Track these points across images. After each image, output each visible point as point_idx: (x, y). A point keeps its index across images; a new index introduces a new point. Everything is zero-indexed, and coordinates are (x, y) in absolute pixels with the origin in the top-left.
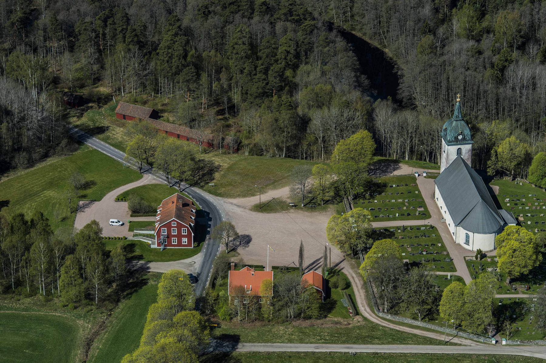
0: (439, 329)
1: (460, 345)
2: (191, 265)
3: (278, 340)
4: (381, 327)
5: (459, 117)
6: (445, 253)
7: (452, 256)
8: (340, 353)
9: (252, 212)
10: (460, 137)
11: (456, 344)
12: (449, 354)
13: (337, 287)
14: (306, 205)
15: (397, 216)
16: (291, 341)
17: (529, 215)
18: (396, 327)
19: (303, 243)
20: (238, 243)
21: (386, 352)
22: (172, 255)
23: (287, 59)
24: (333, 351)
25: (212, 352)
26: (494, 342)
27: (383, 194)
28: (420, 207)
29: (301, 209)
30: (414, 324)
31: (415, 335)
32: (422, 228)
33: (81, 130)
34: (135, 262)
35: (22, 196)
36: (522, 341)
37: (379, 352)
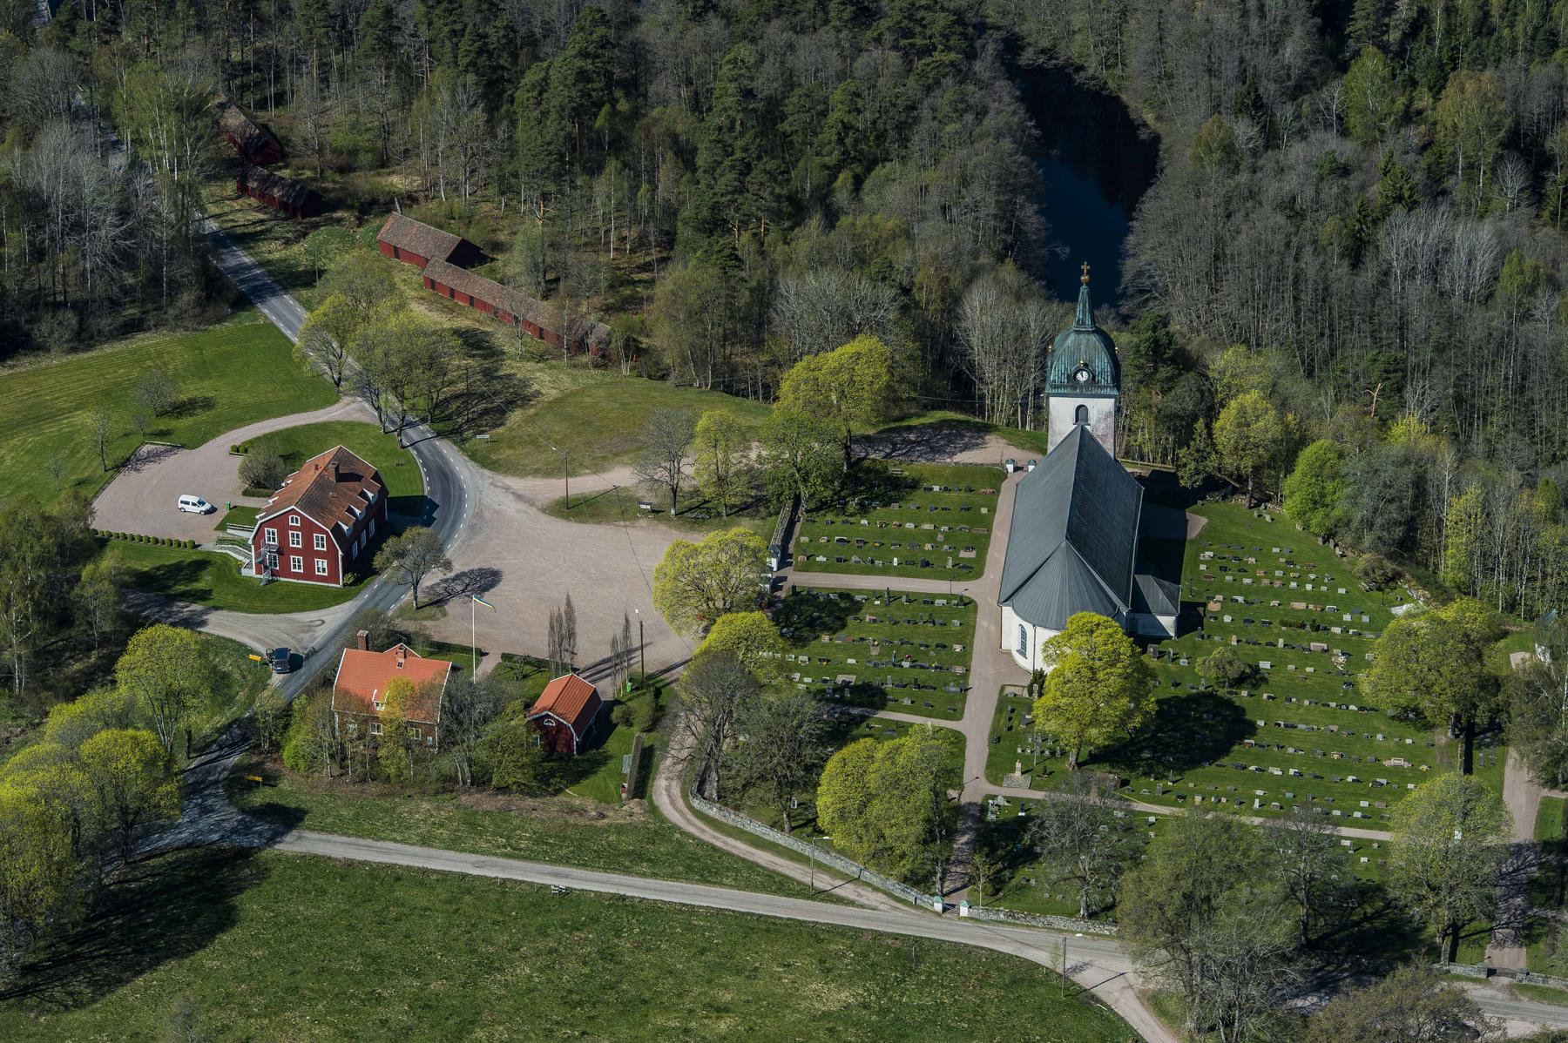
0: (819, 856)
1: (851, 903)
2: (309, 627)
3: (394, 835)
4: (678, 835)
5: (1084, 323)
6: (959, 670)
7: (973, 681)
8: (531, 884)
9: (545, 518)
10: (1083, 377)
11: (840, 900)
12: (805, 922)
13: (631, 725)
14: (682, 513)
15: (895, 563)
16: (425, 841)
17: (1241, 599)
18: (717, 839)
19: (574, 603)
20: (459, 588)
21: (647, 896)
22: (282, 599)
23: (844, 145)
24: (515, 877)
25: (214, 843)
26: (938, 907)
27: (895, 506)
28: (967, 549)
29: (669, 519)
30: (766, 837)
31: (752, 866)
32: (939, 602)
33: (270, 273)
34: (181, 604)
35: (20, 416)
36: (1011, 915)
37: (629, 894)
